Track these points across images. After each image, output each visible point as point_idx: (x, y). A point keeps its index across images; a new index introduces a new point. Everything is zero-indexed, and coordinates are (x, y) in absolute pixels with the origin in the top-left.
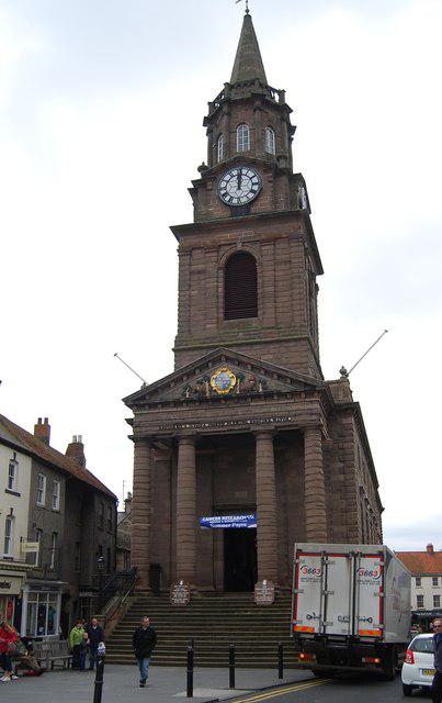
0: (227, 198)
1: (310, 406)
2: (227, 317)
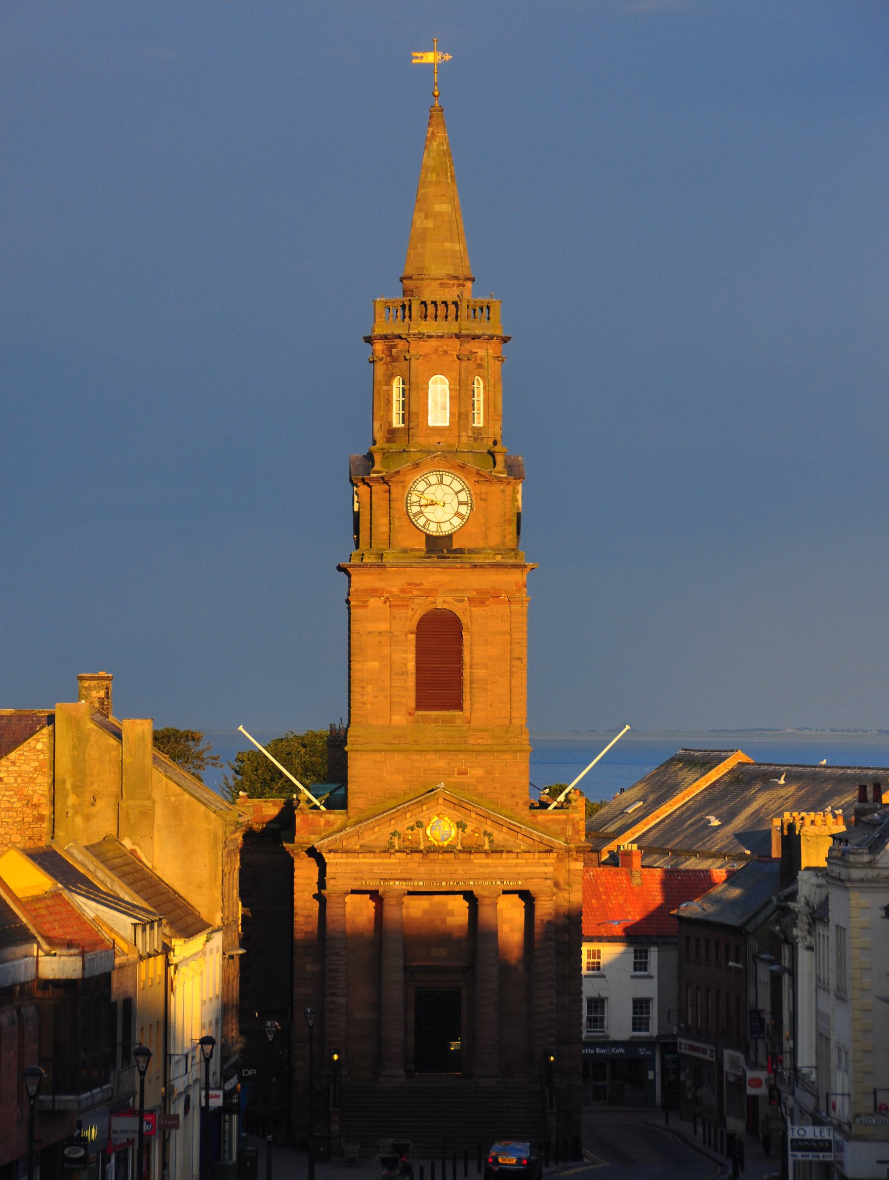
0: (463, 497)
1: (545, 869)
2: (420, 706)
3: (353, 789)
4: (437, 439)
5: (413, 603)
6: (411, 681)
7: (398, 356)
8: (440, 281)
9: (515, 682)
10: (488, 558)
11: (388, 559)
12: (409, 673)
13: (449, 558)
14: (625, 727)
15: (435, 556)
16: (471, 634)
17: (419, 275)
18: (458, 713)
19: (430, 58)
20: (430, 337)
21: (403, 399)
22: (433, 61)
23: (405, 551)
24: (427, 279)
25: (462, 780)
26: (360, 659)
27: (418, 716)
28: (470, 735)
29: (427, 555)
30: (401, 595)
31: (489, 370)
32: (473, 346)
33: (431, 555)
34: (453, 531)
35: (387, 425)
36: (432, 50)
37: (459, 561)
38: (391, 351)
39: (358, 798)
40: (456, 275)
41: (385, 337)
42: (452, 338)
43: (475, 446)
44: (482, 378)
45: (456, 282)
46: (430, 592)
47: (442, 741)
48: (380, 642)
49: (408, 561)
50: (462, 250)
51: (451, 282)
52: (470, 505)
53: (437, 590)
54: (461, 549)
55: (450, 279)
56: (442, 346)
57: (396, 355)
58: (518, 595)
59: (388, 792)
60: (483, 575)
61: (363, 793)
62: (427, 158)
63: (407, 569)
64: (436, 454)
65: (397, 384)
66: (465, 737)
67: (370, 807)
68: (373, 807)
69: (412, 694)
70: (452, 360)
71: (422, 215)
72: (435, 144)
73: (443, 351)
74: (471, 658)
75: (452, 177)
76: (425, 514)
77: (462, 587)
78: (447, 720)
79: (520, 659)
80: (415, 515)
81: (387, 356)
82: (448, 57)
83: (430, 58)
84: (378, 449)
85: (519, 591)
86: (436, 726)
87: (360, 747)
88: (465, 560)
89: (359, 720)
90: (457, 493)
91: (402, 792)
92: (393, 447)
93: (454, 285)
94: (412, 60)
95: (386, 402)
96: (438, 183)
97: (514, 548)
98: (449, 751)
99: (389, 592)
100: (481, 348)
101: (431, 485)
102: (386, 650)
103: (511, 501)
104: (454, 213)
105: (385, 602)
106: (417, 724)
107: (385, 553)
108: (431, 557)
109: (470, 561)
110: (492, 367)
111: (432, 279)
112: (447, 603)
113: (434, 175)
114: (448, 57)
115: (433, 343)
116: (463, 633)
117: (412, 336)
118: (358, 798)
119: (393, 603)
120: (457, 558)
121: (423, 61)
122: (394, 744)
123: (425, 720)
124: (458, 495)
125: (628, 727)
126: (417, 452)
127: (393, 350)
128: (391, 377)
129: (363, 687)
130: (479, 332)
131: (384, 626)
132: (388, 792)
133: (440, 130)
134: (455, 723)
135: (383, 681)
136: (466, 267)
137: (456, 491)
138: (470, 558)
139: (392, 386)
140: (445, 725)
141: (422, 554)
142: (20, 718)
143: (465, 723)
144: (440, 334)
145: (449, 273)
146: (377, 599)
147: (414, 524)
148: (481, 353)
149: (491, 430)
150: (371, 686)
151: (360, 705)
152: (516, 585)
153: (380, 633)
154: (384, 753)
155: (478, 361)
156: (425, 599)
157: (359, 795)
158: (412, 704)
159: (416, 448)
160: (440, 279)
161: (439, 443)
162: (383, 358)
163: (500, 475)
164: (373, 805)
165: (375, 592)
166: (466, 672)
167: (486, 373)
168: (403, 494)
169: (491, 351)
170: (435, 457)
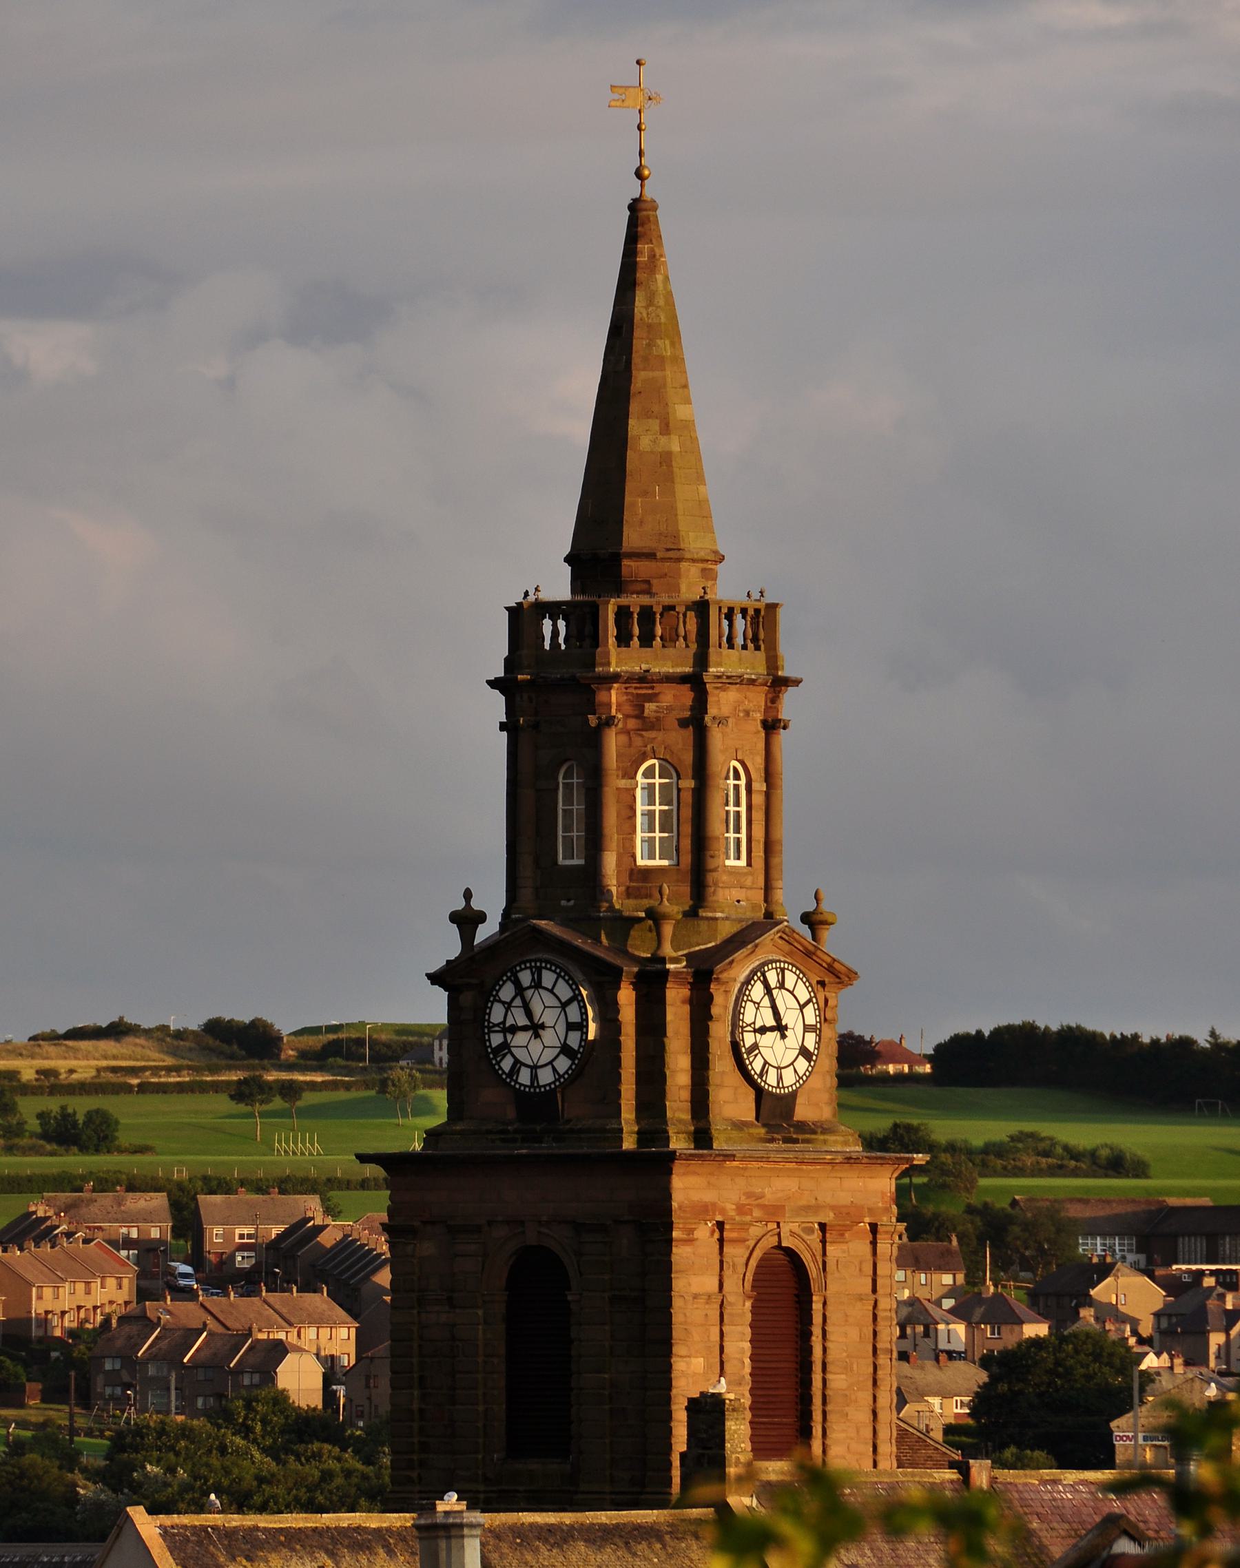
8: (701, 565)
15: (778, 1136)
17: (668, 550)
21: (727, 808)
37: (810, 1147)
38: (642, 708)
48: (706, 1315)
57: (653, 714)
62: (647, 307)
71: (655, 425)
127: (647, 705)
161: (738, 901)
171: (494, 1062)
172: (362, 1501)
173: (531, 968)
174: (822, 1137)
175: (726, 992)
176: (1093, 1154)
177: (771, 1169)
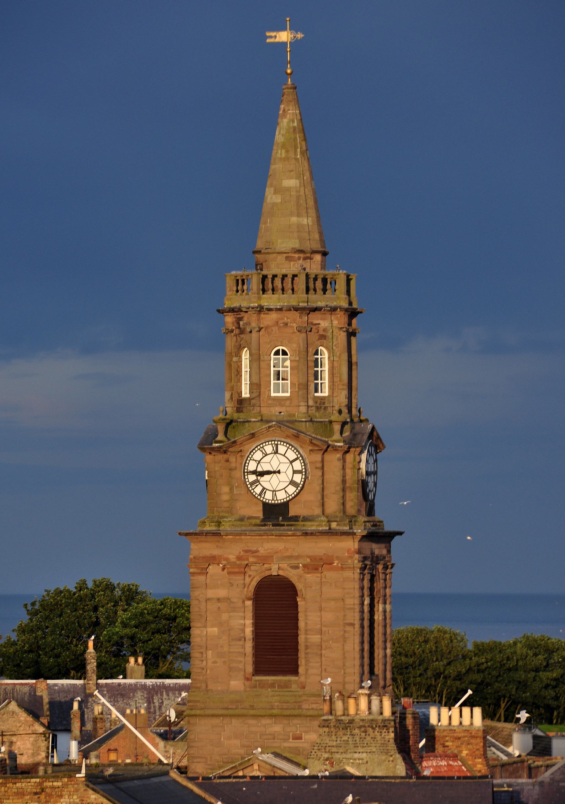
2: (258, 671)
3: (192, 754)
4: (278, 409)
5: (250, 570)
6: (249, 646)
7: (244, 328)
8: (285, 255)
9: (347, 648)
10: (321, 526)
11: (226, 527)
12: (247, 639)
13: (283, 525)
14: (467, 692)
15: (271, 523)
16: (304, 599)
17: (266, 249)
18: (293, 678)
19: (284, 36)
20: (270, 310)
22: (286, 41)
23: (242, 519)
24: (273, 253)
25: (297, 745)
26: (199, 625)
27: (256, 681)
28: (304, 700)
29: (263, 523)
30: (238, 562)
31: (334, 340)
32: (315, 318)
33: (266, 523)
34: (288, 499)
35: (237, 395)
36: (284, 29)
38: (239, 324)
39: (197, 762)
40: (302, 248)
41: (232, 310)
42: (291, 310)
43: (317, 414)
44: (327, 348)
45: (302, 255)
46: (266, 559)
47: (278, 706)
48: (219, 608)
49: (244, 528)
50: (310, 223)
51: (297, 256)
52: (304, 473)
53: (272, 556)
54: (296, 517)
55: (295, 253)
56: (283, 319)
57: (243, 327)
58: (350, 561)
59: (226, 756)
60: (316, 542)
61: (201, 758)
63: (243, 537)
64: (270, 424)
65: (245, 356)
66: (300, 702)
67: (209, 771)
68: (211, 771)
69: (250, 659)
70: (292, 331)
71: (272, 190)
72: (285, 121)
73: (283, 323)
74: (306, 623)
75: (302, 153)
76: (261, 482)
77: (297, 554)
78: (282, 684)
79: (353, 625)
80: (252, 484)
81: (236, 328)
82: (300, 36)
83: (284, 36)
84: (219, 419)
85: (351, 557)
86: (273, 691)
87: (198, 712)
88: (299, 528)
89: (199, 685)
90: (291, 462)
91: (240, 757)
92: (241, 417)
93: (299, 258)
94: (266, 39)
95: (236, 373)
96: (287, 159)
97: (356, 515)
98: (283, 716)
99: (227, 559)
100: (323, 319)
101: (266, 455)
102: (225, 616)
103: (352, 469)
104: (302, 189)
105: (223, 569)
106: (255, 689)
107: (223, 521)
108: (267, 525)
109: (304, 528)
110: (337, 337)
111: (279, 253)
112: (283, 570)
113: (283, 151)
114: (300, 36)
115: (274, 316)
116: (298, 599)
117: (250, 309)
118: (197, 762)
119: (230, 570)
120: (292, 525)
121: (277, 40)
122: (231, 709)
123: (262, 685)
124: (293, 464)
125: (470, 692)
126: (257, 421)
128: (240, 349)
129: (202, 653)
130: (319, 304)
131: (222, 593)
132: (226, 756)
133: (291, 108)
134: (291, 688)
135: (221, 647)
136: (314, 240)
137: (291, 460)
138: (304, 525)
139: (240, 357)
140: (281, 690)
141: (258, 522)
142: (409, 748)
143: (301, 688)
144: (278, 307)
145: (294, 246)
146: (216, 566)
147: (293, 498)
148: (324, 324)
149: (335, 400)
150: (210, 652)
151: (200, 670)
152: (348, 551)
153: (218, 599)
154: (221, 718)
155: (321, 332)
156: (262, 565)
157: (198, 760)
158: (250, 669)
159: (256, 418)
160: (285, 253)
161: (280, 413)
162: (233, 330)
163: (336, 444)
164: (211, 769)
165: (213, 560)
166: (302, 638)
167: (331, 344)
168: (242, 464)
169: (335, 323)
170: (270, 427)
171: (250, 489)
172: (72, 672)
173: (272, 444)
174: (302, 523)
175: (242, 456)
176: (183, 533)
177: (259, 539)
